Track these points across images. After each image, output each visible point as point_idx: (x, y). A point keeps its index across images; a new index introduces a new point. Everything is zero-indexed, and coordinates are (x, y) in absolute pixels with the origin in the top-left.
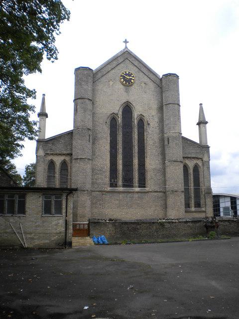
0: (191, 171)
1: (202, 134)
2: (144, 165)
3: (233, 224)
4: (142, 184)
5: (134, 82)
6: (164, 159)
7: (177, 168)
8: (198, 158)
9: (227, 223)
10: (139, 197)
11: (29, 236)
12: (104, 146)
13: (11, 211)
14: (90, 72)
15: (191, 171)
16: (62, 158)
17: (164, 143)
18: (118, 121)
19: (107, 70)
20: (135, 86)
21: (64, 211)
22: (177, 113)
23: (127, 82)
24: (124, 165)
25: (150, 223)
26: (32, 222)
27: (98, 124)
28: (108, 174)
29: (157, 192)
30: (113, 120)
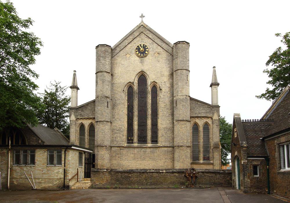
0: (201, 129)
1: (214, 96)
2: (157, 125)
3: (218, 176)
4: (155, 140)
5: (148, 53)
6: (173, 119)
7: (183, 126)
8: (208, 117)
9: (212, 175)
10: (151, 152)
11: (37, 181)
12: (122, 111)
13: (26, 163)
14: (107, 48)
15: (201, 129)
16: (90, 121)
17: (173, 104)
18: (134, 88)
19: (125, 45)
20: (149, 57)
21: (63, 162)
22: (185, 78)
23: (142, 52)
24: (139, 125)
25: (140, 172)
26: (40, 170)
27: (117, 92)
28: (125, 133)
29: (167, 147)
30: (130, 87)
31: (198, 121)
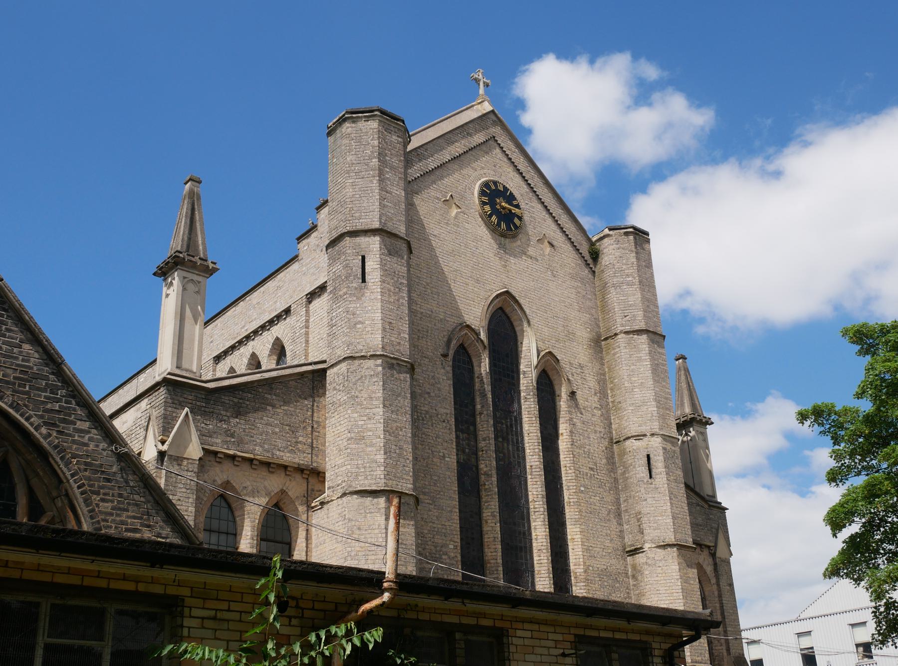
31: (242, 478)
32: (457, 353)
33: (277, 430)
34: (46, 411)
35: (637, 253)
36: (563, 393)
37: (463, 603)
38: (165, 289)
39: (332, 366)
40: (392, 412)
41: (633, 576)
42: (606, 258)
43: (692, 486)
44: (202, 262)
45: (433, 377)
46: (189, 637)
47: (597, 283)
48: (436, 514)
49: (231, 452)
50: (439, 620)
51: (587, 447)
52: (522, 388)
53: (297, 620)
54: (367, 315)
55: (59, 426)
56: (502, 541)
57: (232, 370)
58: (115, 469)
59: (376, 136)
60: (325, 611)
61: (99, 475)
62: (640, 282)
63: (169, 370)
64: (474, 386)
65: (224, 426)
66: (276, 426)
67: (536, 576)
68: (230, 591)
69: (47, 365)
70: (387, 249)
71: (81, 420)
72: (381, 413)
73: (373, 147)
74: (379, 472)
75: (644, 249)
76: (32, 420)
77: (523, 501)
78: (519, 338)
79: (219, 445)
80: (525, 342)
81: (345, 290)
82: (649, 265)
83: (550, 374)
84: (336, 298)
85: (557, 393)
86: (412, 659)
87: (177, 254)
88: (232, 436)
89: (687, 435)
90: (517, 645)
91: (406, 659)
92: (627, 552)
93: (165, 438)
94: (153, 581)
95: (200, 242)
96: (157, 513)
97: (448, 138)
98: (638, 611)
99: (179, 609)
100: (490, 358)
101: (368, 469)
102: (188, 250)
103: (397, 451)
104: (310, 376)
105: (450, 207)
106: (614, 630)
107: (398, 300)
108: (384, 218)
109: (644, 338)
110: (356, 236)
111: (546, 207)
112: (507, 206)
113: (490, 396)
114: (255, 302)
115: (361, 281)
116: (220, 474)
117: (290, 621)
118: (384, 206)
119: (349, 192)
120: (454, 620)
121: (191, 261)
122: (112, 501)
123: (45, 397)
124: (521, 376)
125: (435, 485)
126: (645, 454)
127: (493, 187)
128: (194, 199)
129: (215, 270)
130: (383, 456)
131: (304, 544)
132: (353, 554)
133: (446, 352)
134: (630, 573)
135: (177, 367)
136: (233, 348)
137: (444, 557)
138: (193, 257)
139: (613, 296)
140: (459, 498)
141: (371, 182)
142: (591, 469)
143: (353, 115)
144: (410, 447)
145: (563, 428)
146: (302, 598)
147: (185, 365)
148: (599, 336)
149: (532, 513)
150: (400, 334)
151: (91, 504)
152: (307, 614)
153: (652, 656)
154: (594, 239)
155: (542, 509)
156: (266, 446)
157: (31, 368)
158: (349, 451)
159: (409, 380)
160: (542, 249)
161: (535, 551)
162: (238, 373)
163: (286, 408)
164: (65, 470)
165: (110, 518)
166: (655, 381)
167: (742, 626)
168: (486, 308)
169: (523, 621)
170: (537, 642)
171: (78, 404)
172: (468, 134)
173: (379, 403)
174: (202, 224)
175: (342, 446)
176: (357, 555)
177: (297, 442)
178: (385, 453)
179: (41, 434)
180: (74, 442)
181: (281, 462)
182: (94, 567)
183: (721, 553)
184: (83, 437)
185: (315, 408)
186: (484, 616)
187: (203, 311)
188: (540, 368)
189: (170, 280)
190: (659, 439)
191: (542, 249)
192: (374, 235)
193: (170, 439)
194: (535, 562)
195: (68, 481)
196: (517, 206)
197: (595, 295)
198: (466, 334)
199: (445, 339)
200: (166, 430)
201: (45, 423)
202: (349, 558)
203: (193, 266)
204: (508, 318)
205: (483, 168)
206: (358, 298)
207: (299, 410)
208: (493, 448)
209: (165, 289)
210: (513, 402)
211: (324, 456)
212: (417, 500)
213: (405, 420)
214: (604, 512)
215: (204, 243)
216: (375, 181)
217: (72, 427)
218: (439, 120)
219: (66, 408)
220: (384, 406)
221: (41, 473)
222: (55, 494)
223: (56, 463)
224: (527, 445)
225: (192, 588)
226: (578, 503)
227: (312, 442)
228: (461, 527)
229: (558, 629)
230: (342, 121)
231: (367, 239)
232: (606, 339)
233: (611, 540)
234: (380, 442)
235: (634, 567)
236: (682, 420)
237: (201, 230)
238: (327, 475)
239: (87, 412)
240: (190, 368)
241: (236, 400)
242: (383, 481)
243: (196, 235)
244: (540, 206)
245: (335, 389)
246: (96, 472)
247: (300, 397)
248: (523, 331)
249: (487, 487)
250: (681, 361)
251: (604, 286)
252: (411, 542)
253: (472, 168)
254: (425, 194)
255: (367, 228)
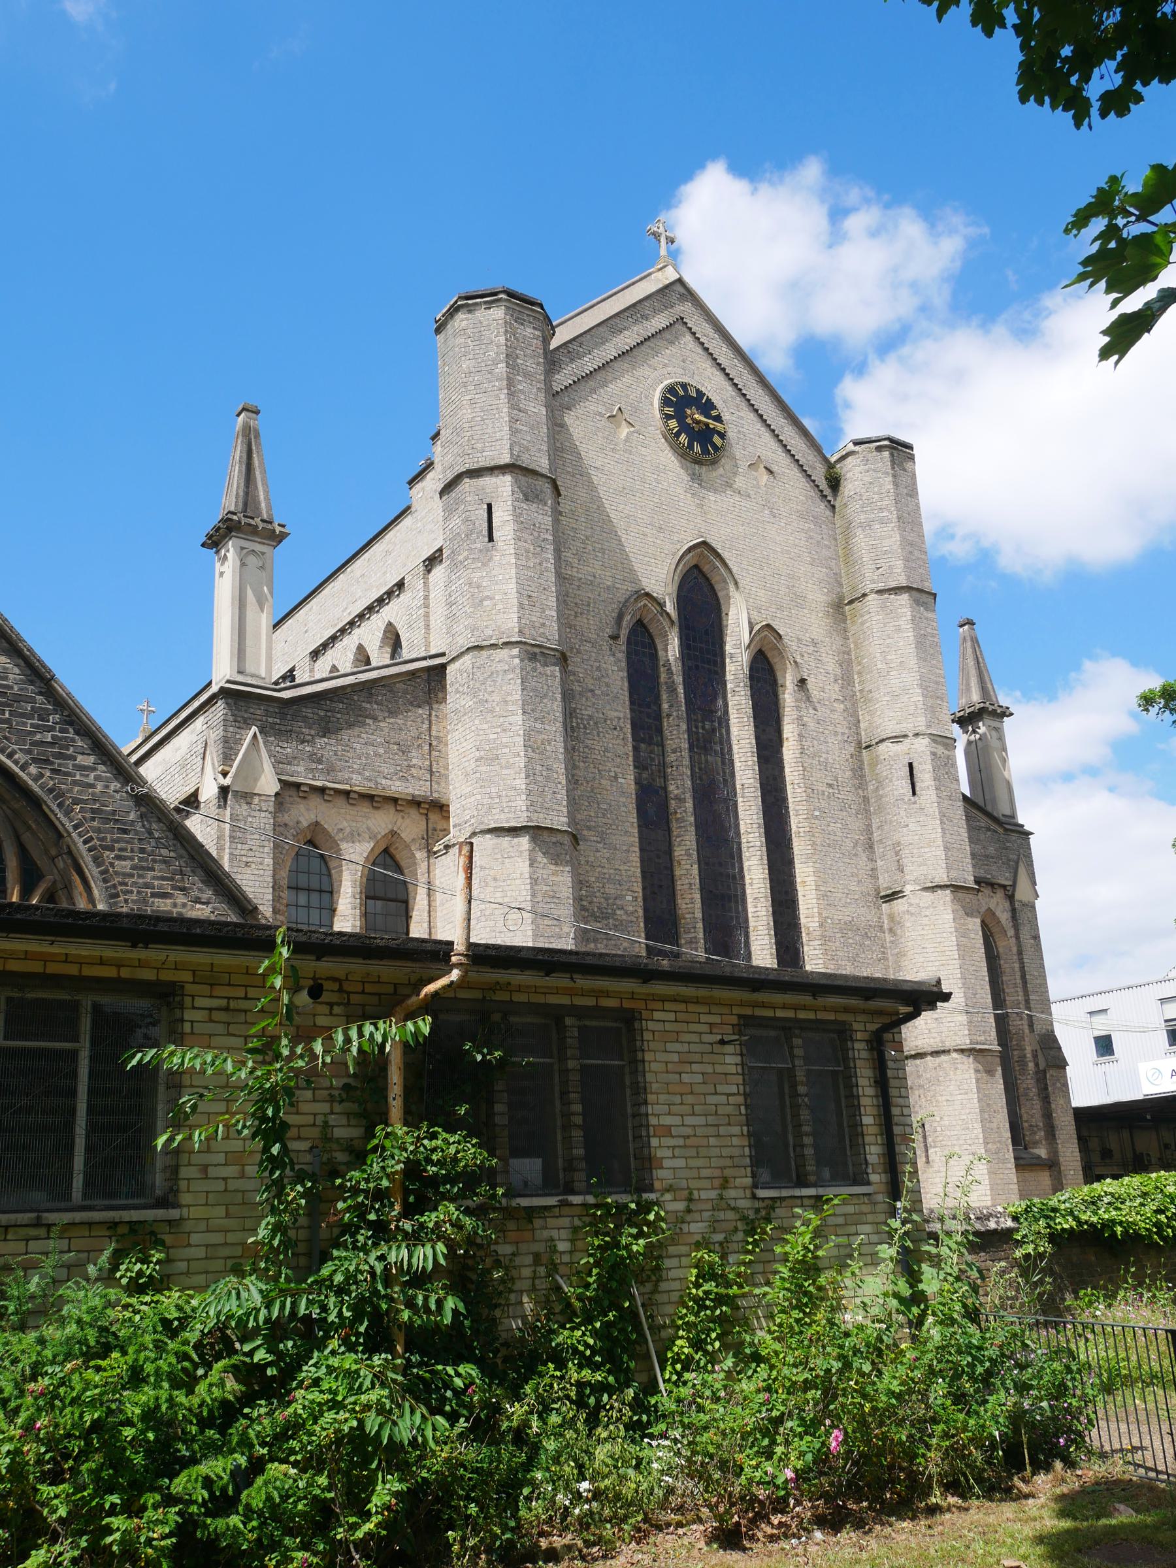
31: (335, 818)
32: (633, 632)
33: (381, 751)
34: (35, 743)
35: (894, 476)
36: (789, 681)
37: (572, 978)
38: (218, 565)
39: (453, 660)
40: (536, 719)
41: (891, 930)
42: (850, 486)
43: (981, 803)
44: (265, 525)
45: (598, 668)
46: (192, 1033)
47: (838, 523)
48: (607, 855)
49: (319, 783)
50: (542, 1001)
51: (824, 756)
52: (729, 677)
53: (342, 1007)
54: (497, 587)
55: (53, 763)
56: (702, 889)
57: (334, 668)
58: (132, 816)
59: (502, 330)
60: (379, 995)
61: (112, 825)
62: (899, 518)
63: (228, 677)
64: (658, 677)
65: (308, 749)
66: (379, 745)
67: (752, 934)
68: (247, 973)
69: (32, 683)
70: (522, 492)
71: (83, 754)
72: (520, 722)
73: (498, 346)
74: (520, 803)
75: (905, 470)
76: (16, 756)
77: (732, 833)
78: (723, 608)
79: (301, 774)
80: (732, 612)
81: (466, 553)
82: (913, 492)
83: (769, 655)
84: (455, 566)
85: (780, 682)
86: (496, 1054)
87: (230, 516)
88: (319, 761)
89: (974, 732)
90: (653, 1032)
91: (490, 1053)
92: (882, 897)
93: (227, 768)
94: (141, 964)
95: (262, 497)
96: (193, 871)
97: (612, 324)
98: (829, 982)
99: (178, 999)
100: (681, 638)
101: (504, 800)
102: (245, 511)
103: (544, 773)
104: (425, 675)
105: (619, 426)
106: (796, 1008)
107: (540, 564)
108: (517, 449)
109: (905, 597)
110: (478, 477)
111: (761, 416)
112: (703, 419)
113: (681, 690)
114: (358, 573)
115: (487, 539)
116: (305, 813)
117: (331, 1009)
118: (517, 431)
119: (467, 413)
120: (565, 1000)
121: (250, 525)
122: (132, 859)
123: (32, 725)
124: (728, 660)
125: (604, 815)
126: (906, 762)
127: (682, 393)
128: (250, 437)
129: (283, 536)
130: (524, 781)
131: (426, 902)
132: (487, 913)
133: (616, 632)
134: (886, 926)
135: (239, 672)
136: (334, 639)
137: (618, 912)
138: (252, 518)
139: (861, 540)
140: (640, 832)
141: (497, 396)
142: (830, 786)
143: (468, 301)
144: (563, 766)
145: (789, 730)
146: (347, 979)
147: (250, 668)
148: (841, 599)
149: (744, 850)
150: (544, 612)
151: (103, 863)
152: (355, 999)
153: (852, 1040)
154: (833, 460)
155: (758, 844)
156: (367, 774)
157: (11, 688)
158: (478, 775)
159: (558, 674)
160: (755, 478)
161: (749, 900)
162: (342, 672)
163: (392, 720)
164: (64, 820)
165: (130, 881)
166: (920, 658)
167: (1053, 996)
168: (673, 567)
169: (664, 999)
170: (684, 1027)
171: (77, 733)
172: (642, 316)
173: (517, 708)
174: (264, 472)
175: (469, 769)
176: (492, 914)
177: (409, 766)
178: (527, 777)
179: (29, 774)
180: (75, 783)
181: (388, 794)
182: (55, 949)
183: (1021, 894)
184: (87, 776)
185: (433, 718)
186: (608, 994)
187: (272, 593)
188: (755, 650)
189: (223, 552)
190: (925, 741)
191: (755, 478)
192: (504, 474)
193: (233, 770)
194: (750, 915)
195: (69, 835)
196: (718, 419)
197: (836, 540)
198: (645, 605)
199: (615, 615)
200: (227, 757)
201: (35, 760)
202: (483, 919)
203: (253, 531)
204: (707, 579)
205: (666, 365)
206: (485, 564)
207: (412, 722)
208: (686, 762)
209: (218, 565)
210: (715, 698)
211: (447, 783)
212: (575, 839)
213: (554, 730)
214: (849, 844)
215: (267, 499)
216: (503, 396)
217: (71, 763)
218: (599, 299)
219: (61, 739)
220: (524, 712)
221: (34, 826)
222: (53, 852)
223: (52, 811)
224: (736, 757)
225: (194, 971)
226: (811, 833)
227: (431, 765)
228: (643, 872)
229: (714, 1009)
230: (454, 310)
231: (494, 479)
232: (851, 602)
233: (859, 882)
234: (520, 762)
235: (892, 918)
236: (968, 711)
237: (262, 480)
238: (452, 809)
239: (90, 742)
240: (257, 673)
241: (322, 713)
242: (525, 814)
243: (256, 488)
244: (752, 416)
245: (457, 691)
246: (107, 821)
247: (411, 704)
248: (728, 597)
249: (679, 816)
250: (966, 627)
251: (848, 526)
252: (566, 895)
253: (650, 366)
254: (579, 410)
255: (493, 464)
